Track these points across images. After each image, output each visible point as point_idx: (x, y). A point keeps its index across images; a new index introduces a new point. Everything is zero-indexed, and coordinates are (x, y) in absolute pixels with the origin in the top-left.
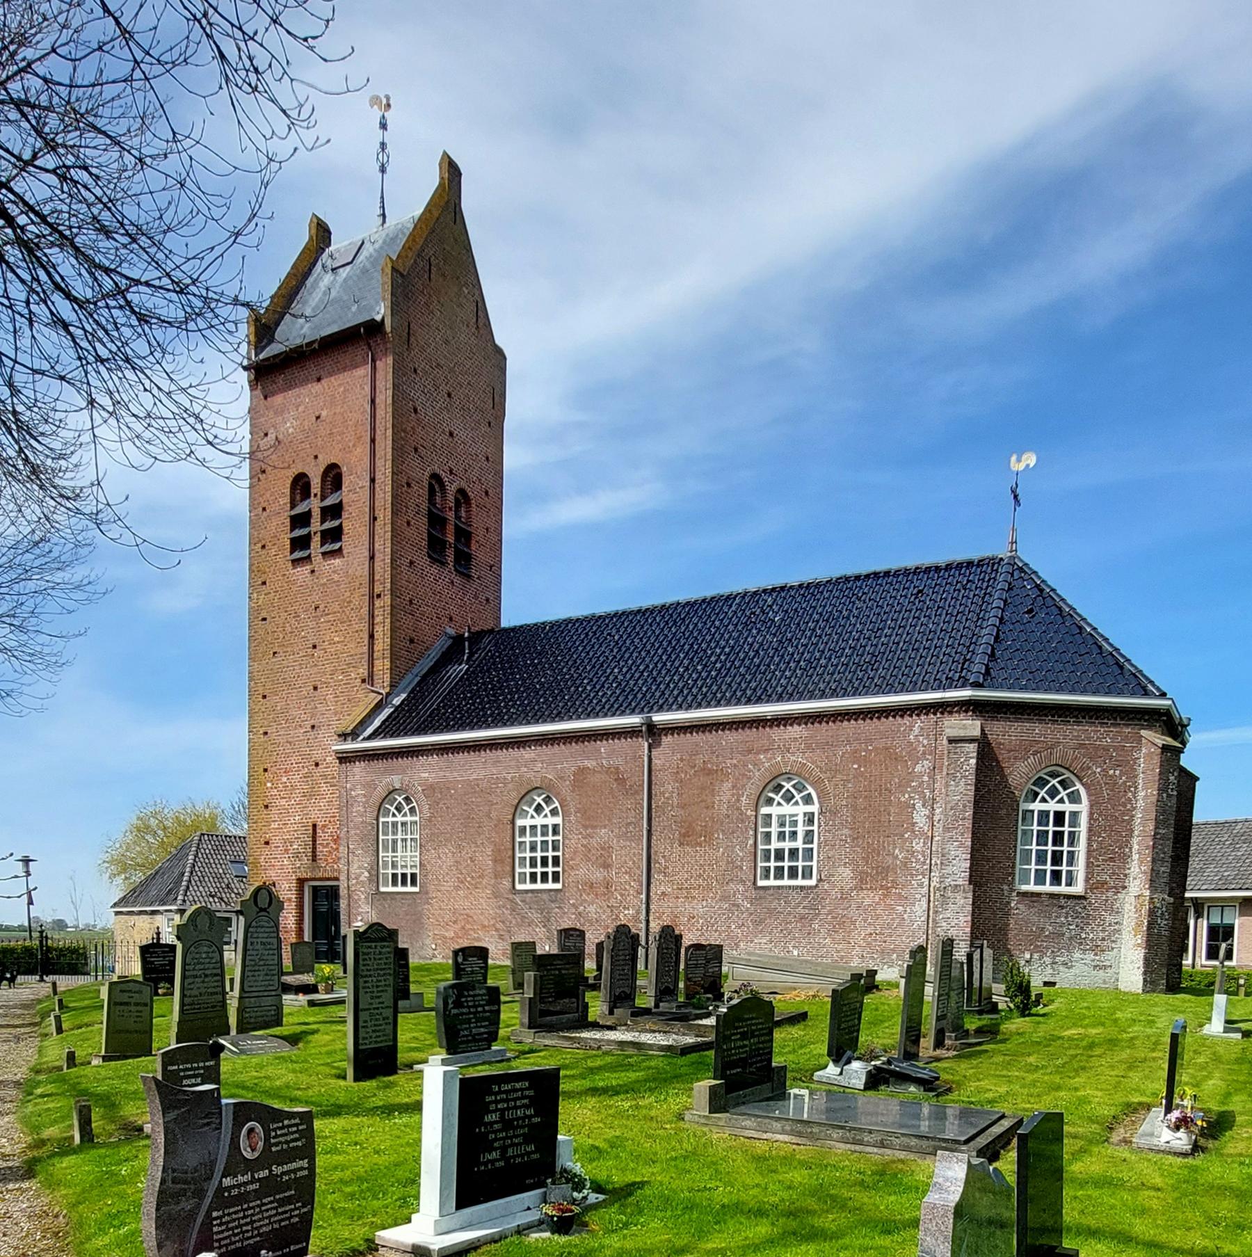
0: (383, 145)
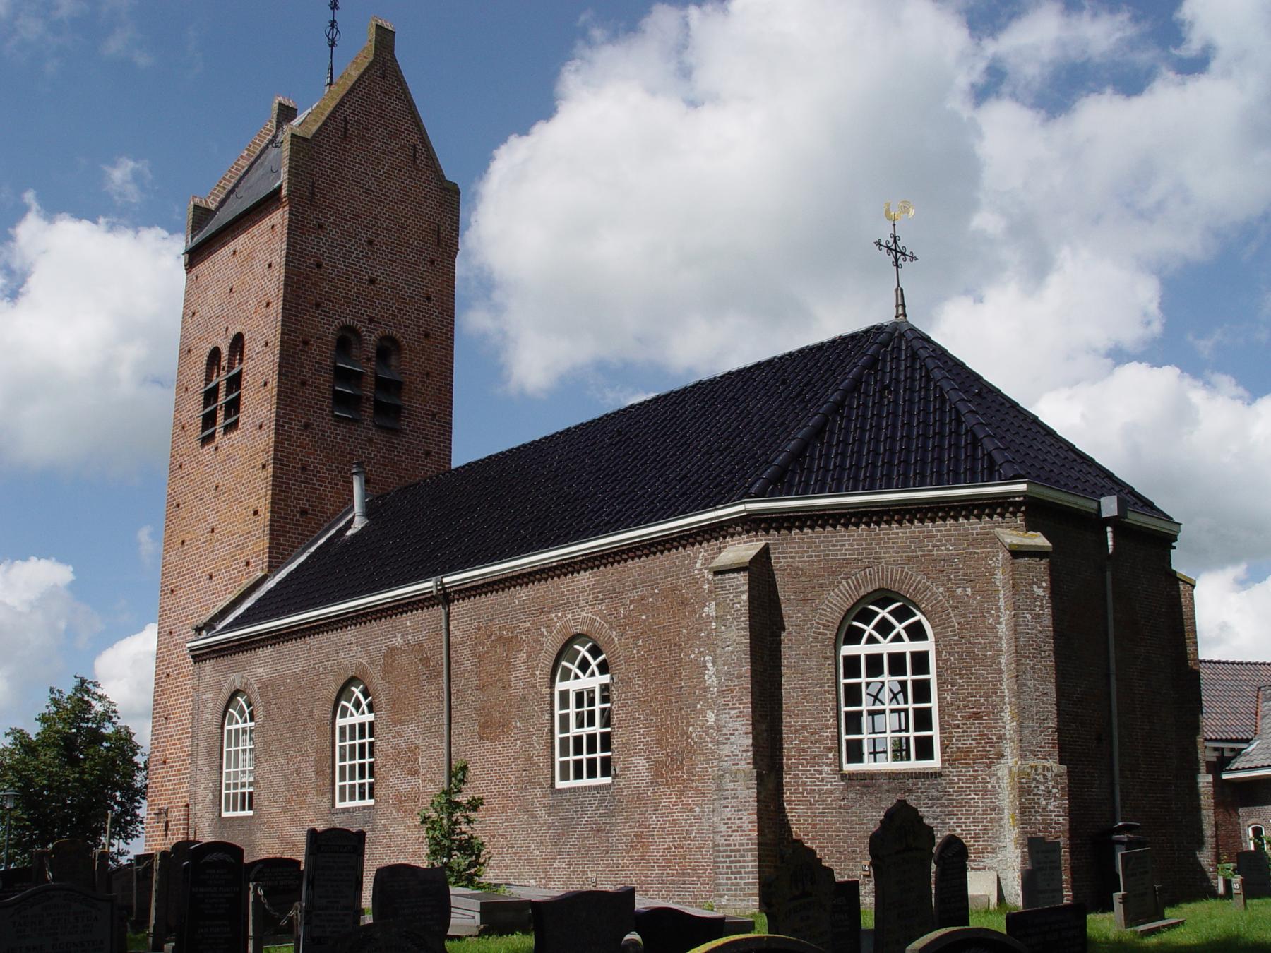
0: (333, 23)
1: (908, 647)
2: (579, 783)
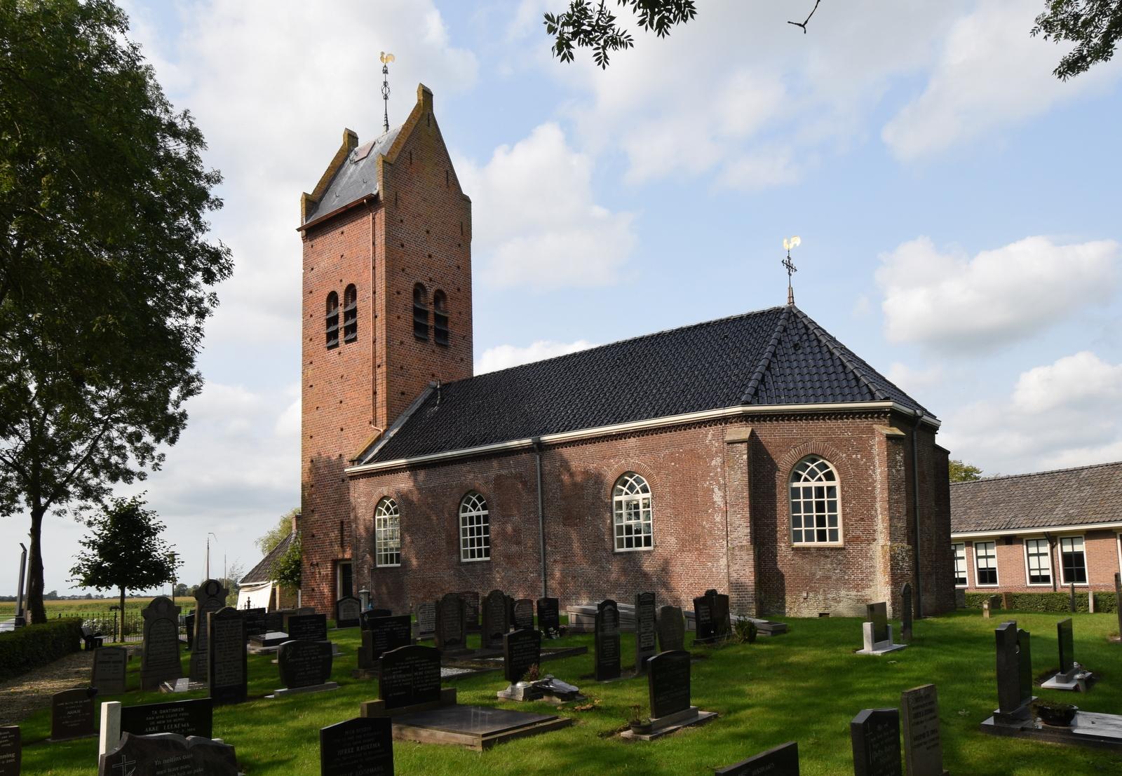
0: (385, 84)
1: (825, 484)
2: (479, 559)
